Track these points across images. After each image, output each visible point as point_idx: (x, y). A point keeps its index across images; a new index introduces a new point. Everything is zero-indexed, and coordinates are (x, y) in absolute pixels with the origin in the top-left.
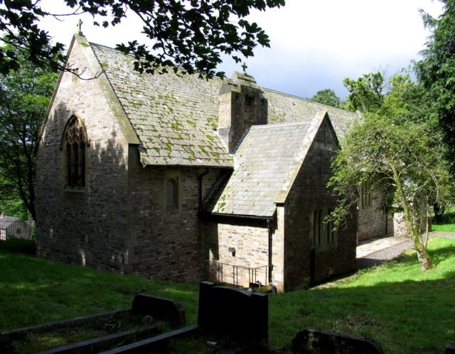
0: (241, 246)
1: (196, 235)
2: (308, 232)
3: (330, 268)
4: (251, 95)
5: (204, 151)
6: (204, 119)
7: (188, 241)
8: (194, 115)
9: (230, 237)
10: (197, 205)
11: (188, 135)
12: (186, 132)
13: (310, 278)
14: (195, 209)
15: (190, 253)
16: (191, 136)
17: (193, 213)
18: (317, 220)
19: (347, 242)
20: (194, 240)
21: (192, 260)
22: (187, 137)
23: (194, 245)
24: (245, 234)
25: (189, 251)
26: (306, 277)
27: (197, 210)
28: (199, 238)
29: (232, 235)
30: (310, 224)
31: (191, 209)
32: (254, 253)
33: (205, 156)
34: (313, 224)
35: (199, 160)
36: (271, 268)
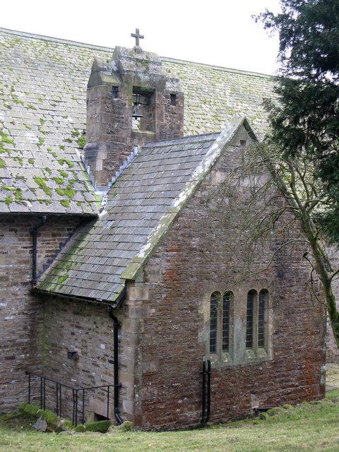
0: (84, 350)
1: (25, 328)
2: (194, 332)
3: (253, 396)
4: (147, 86)
5: (42, 186)
6: (67, 131)
7: (8, 338)
8: (46, 124)
9: (73, 334)
10: (28, 278)
11: (20, 160)
12: (15, 155)
13: (200, 411)
14: (25, 284)
15: (13, 358)
16: (25, 161)
17: (22, 292)
18: (220, 310)
19: (299, 351)
20: (21, 336)
21: (17, 370)
22: (17, 163)
23: (20, 344)
24: (90, 329)
25: (11, 354)
26: (190, 409)
27: (29, 287)
28: (33, 334)
29: (75, 330)
30: (200, 318)
31: (16, 284)
32: (100, 363)
33: (41, 195)
34: (207, 317)
35: (29, 204)
36: (118, 387)
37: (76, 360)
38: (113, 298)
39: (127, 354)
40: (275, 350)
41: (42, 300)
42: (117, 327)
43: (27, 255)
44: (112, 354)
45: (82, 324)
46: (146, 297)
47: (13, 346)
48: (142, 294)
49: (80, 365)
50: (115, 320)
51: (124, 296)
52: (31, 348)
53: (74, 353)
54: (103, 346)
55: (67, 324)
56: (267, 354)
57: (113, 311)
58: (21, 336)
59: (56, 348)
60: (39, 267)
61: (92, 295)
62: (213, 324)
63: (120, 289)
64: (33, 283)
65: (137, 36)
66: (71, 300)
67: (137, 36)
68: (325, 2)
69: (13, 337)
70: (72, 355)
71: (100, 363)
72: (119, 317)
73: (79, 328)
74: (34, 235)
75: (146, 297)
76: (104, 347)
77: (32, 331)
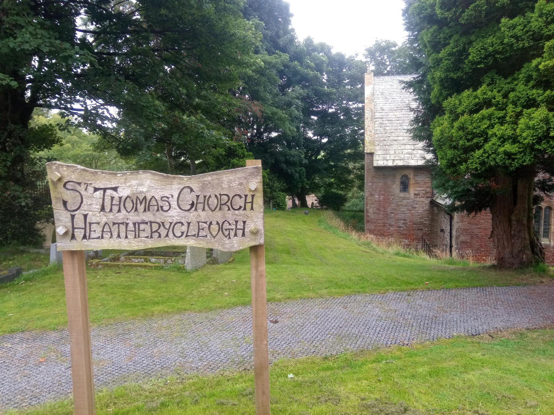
20: (426, 220)
39: (454, 233)
58: (426, 220)
69: (422, 220)
77: (432, 219)
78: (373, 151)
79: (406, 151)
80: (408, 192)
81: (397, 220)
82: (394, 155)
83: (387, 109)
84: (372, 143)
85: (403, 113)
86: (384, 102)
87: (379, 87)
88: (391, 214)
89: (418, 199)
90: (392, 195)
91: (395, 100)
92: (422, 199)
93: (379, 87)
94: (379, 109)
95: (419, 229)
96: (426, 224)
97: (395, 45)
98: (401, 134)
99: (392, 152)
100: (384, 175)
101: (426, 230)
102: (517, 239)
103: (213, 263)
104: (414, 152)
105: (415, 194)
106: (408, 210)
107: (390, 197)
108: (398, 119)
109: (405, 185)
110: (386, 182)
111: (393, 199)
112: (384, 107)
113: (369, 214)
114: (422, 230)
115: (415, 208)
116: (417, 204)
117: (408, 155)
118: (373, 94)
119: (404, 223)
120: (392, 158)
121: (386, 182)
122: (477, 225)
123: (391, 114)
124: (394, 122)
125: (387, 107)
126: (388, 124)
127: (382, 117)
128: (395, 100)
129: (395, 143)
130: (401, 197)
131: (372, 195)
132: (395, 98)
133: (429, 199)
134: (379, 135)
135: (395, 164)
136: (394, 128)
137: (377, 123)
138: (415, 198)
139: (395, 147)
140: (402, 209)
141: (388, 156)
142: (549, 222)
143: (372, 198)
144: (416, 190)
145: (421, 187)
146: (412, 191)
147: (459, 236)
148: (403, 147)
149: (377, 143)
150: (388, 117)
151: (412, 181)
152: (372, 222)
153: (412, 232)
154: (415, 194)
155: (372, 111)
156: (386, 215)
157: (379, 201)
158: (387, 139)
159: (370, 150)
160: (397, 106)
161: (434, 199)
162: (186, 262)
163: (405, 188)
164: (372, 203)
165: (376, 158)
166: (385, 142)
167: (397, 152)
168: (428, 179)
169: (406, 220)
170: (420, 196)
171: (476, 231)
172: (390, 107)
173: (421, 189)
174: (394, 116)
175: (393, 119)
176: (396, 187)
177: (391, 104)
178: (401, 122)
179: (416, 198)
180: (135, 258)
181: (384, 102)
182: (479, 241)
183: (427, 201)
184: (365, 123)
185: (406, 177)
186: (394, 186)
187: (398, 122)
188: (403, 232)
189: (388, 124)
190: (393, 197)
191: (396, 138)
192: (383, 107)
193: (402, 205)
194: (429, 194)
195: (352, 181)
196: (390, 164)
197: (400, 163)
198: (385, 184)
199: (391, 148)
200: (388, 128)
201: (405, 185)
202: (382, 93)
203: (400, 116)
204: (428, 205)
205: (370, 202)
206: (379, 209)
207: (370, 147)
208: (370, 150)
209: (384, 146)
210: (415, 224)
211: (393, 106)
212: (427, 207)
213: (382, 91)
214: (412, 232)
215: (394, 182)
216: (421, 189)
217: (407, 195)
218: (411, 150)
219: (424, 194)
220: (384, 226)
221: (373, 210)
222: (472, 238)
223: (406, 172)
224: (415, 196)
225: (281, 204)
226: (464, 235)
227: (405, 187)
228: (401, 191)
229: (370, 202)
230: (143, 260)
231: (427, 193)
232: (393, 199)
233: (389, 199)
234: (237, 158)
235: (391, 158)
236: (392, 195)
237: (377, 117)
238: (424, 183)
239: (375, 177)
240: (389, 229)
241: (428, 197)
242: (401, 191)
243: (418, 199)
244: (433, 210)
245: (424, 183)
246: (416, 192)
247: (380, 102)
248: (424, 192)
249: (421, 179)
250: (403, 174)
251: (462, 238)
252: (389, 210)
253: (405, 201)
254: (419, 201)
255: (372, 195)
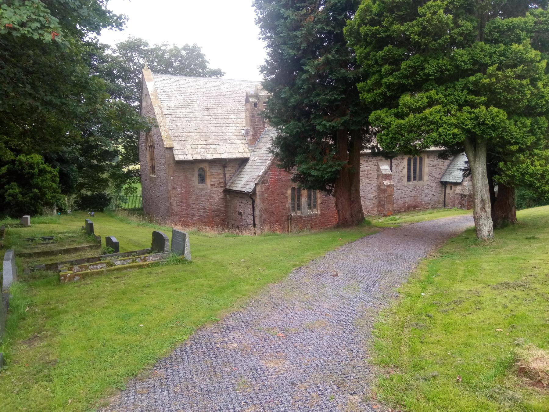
20: (221, 207)
28: (226, 206)
29: (241, 204)
32: (249, 216)
37: (242, 215)
38: (251, 191)
39: (257, 213)
40: (321, 210)
41: (228, 192)
42: (253, 202)
43: (222, 176)
44: (252, 212)
45: (243, 202)
46: (263, 190)
47: (218, 211)
48: (262, 189)
49: (243, 217)
50: (252, 199)
51: (254, 190)
52: (226, 212)
53: (241, 213)
54: (250, 210)
55: (238, 202)
56: (317, 212)
57: (251, 196)
58: (221, 207)
59: (235, 211)
60: (227, 179)
61: (244, 190)
62: (293, 199)
63: (253, 187)
64: (225, 186)
65: (264, 48)
66: (239, 193)
67: (264, 48)
68: (548, 298)
69: (218, 208)
70: (240, 214)
71: (249, 216)
72: (254, 198)
73: (242, 203)
74: (224, 167)
75: (263, 190)
76: (250, 210)
77: (226, 205)
78: (172, 146)
79: (200, 146)
80: (205, 183)
81: (198, 209)
82: (191, 150)
83: (173, 106)
84: (169, 138)
85: (188, 111)
86: (168, 100)
87: (159, 84)
88: (192, 205)
89: (214, 189)
90: (192, 187)
91: (177, 98)
92: (217, 189)
93: (159, 84)
94: (166, 106)
95: (216, 216)
96: (222, 210)
97: (146, 45)
98: (192, 130)
99: (189, 147)
100: (183, 169)
101: (222, 216)
102: (355, 204)
103: (395, 213)
104: (208, 147)
105: (212, 185)
106: (207, 199)
107: (190, 189)
108: (185, 116)
109: (202, 178)
110: (186, 175)
111: (193, 191)
112: (170, 104)
113: (173, 207)
114: (219, 216)
115: (212, 197)
116: (213, 194)
117: (204, 150)
118: (156, 91)
119: (204, 212)
120: (190, 152)
121: (186, 175)
122: (273, 204)
123: (177, 111)
124: (183, 119)
125: (172, 104)
126: (178, 121)
127: (170, 113)
128: (177, 98)
129: (189, 138)
130: (200, 189)
131: (174, 188)
132: (177, 96)
133: (223, 188)
134: (173, 131)
135: (194, 158)
136: (185, 124)
137: (167, 119)
138: (212, 188)
139: (190, 142)
140: (202, 200)
141: (186, 150)
142: (316, 197)
143: (175, 191)
144: (212, 181)
145: (215, 178)
146: (209, 182)
147: (262, 215)
148: (197, 142)
149: (173, 138)
150: (176, 113)
151: (208, 174)
152: (176, 215)
153: (211, 219)
154: (212, 185)
155: (160, 107)
156: (189, 207)
157: (181, 193)
158: (181, 135)
159: (169, 145)
160: (181, 104)
161: (227, 187)
162: (186, 252)
163: (202, 180)
164: (175, 197)
165: (175, 152)
166: (179, 137)
167: (193, 147)
168: (220, 171)
169: (205, 209)
170: (216, 186)
171: (273, 210)
172: (175, 104)
173: (216, 180)
174: (181, 114)
175: (182, 116)
176: (195, 180)
177: (175, 102)
178: (189, 119)
179: (213, 188)
180: (93, 265)
181: (168, 100)
182: (275, 217)
183: (221, 190)
184: (157, 119)
185: (202, 169)
186: (194, 179)
187: (186, 119)
188: (204, 220)
189: (178, 121)
190: (193, 189)
191: (189, 134)
192: (168, 104)
193: (201, 196)
194: (222, 183)
195: (105, 181)
196: (190, 158)
197: (199, 157)
198: (186, 177)
199: (187, 144)
200: (178, 124)
201: (202, 178)
202: (164, 91)
203: (187, 113)
204: (222, 193)
205: (173, 195)
206: (182, 202)
207: (169, 143)
208: (169, 145)
209: (181, 142)
210: (213, 212)
211: (177, 104)
212: (222, 196)
213: (163, 89)
214: (211, 219)
215: (193, 175)
216: (216, 180)
217: (204, 186)
218: (204, 146)
219: (218, 184)
220: (187, 217)
221: (177, 203)
222: (270, 215)
223: (202, 165)
224: (212, 187)
225: (63, 208)
226: (265, 214)
227: (202, 179)
228: (199, 183)
229: (173, 195)
230: (104, 265)
231: (221, 183)
232: (193, 191)
233: (190, 191)
234: (24, 155)
235: (190, 153)
236: (192, 187)
237: (166, 113)
238: (218, 174)
239: (176, 171)
240: (192, 219)
241: (221, 187)
242: (199, 183)
243: (214, 189)
244: (226, 198)
245: (218, 174)
246: (212, 183)
247: (164, 100)
248: (218, 182)
249: (215, 171)
250: (200, 167)
251: (264, 216)
252: (191, 201)
253: (204, 192)
254: (215, 191)
255: (174, 188)
